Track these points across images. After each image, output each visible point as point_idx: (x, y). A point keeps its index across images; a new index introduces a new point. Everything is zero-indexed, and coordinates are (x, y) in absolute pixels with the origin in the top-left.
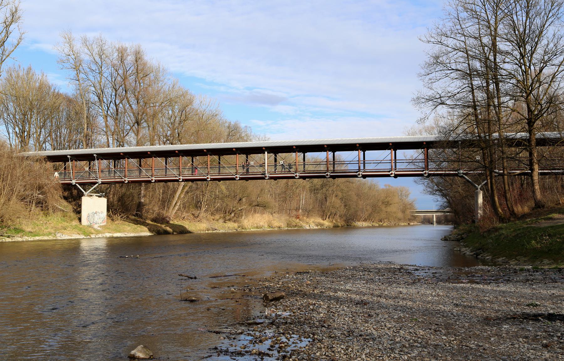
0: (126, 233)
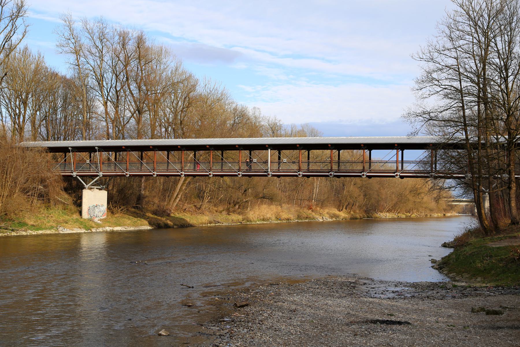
0: (126, 227)
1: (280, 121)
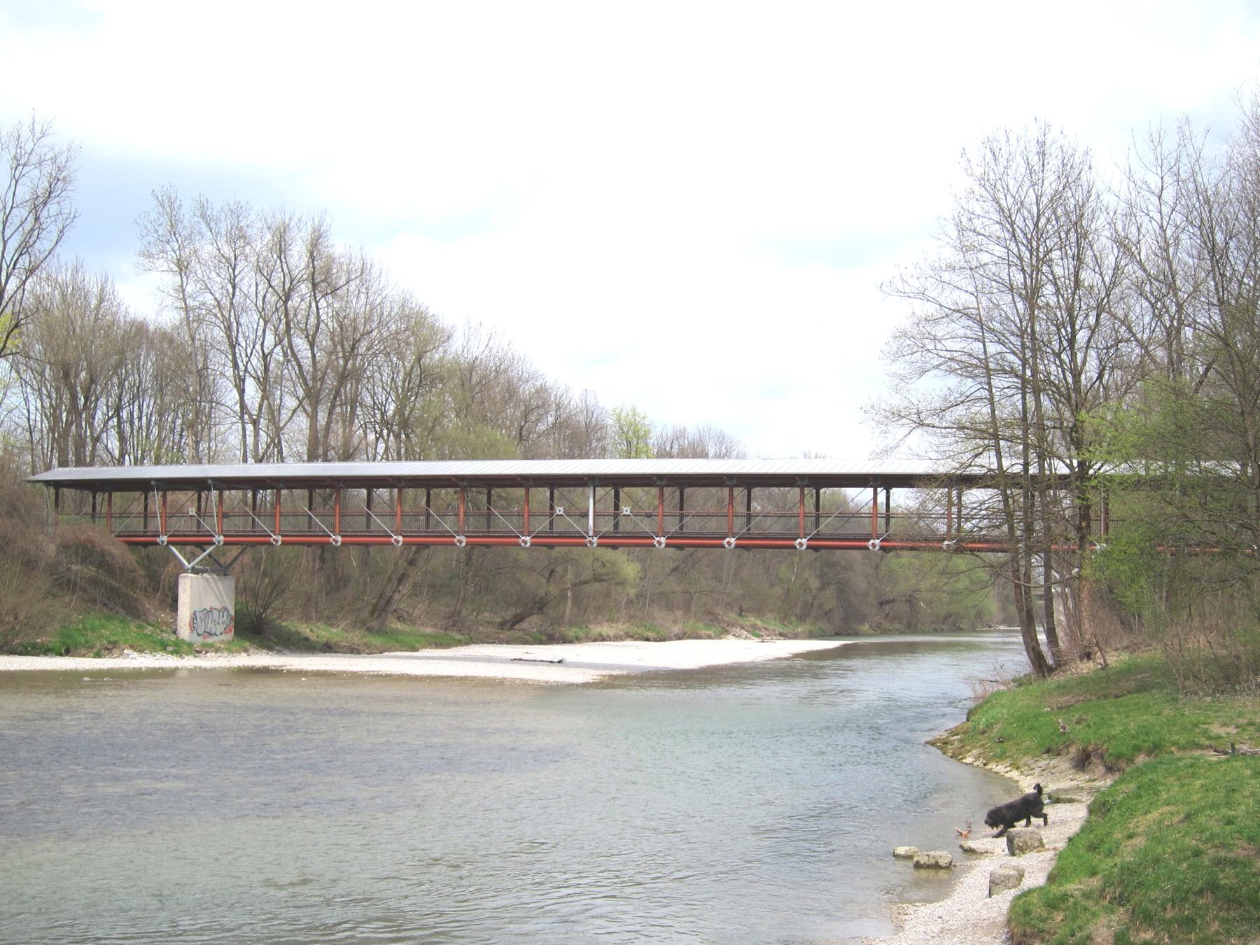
1: (644, 418)
